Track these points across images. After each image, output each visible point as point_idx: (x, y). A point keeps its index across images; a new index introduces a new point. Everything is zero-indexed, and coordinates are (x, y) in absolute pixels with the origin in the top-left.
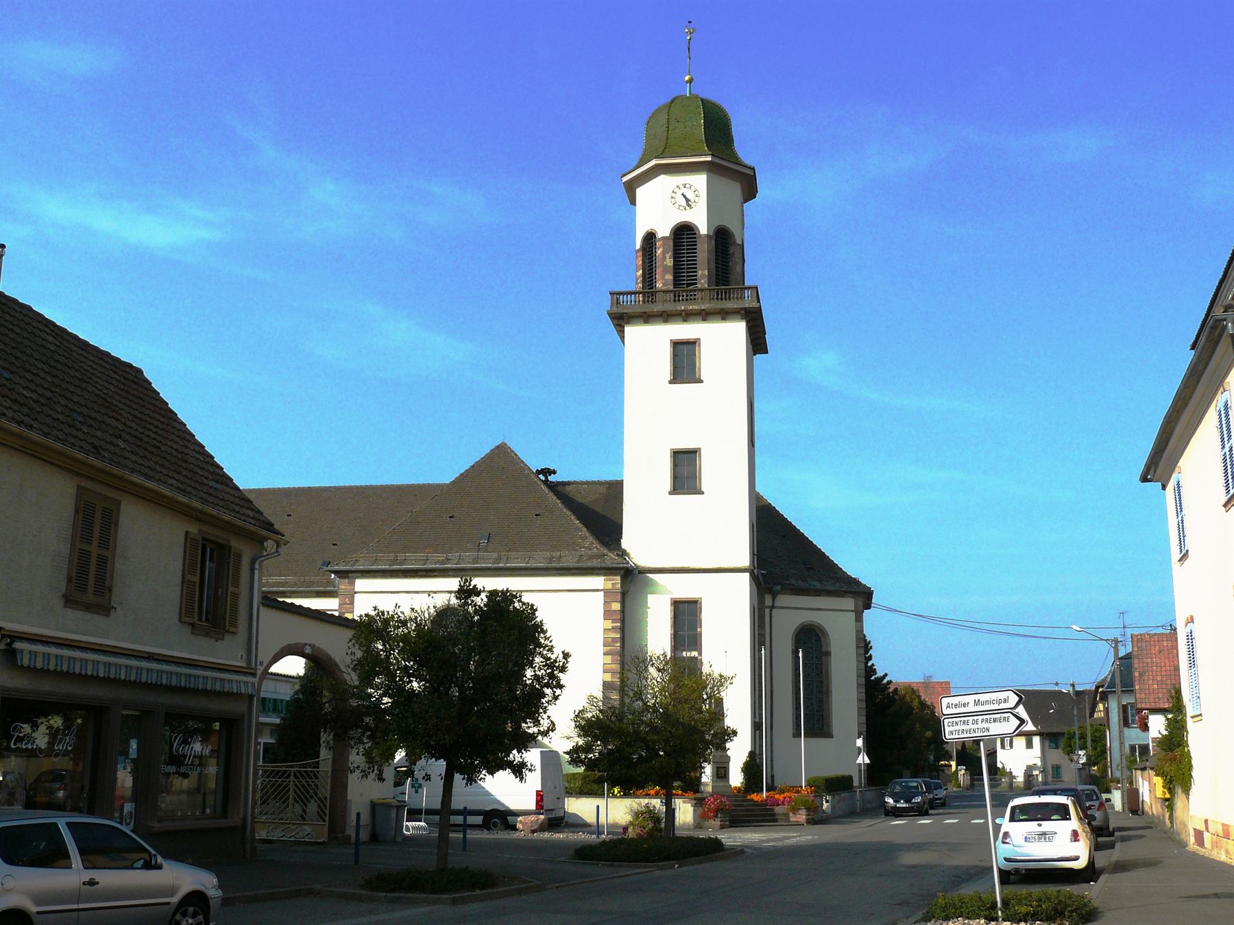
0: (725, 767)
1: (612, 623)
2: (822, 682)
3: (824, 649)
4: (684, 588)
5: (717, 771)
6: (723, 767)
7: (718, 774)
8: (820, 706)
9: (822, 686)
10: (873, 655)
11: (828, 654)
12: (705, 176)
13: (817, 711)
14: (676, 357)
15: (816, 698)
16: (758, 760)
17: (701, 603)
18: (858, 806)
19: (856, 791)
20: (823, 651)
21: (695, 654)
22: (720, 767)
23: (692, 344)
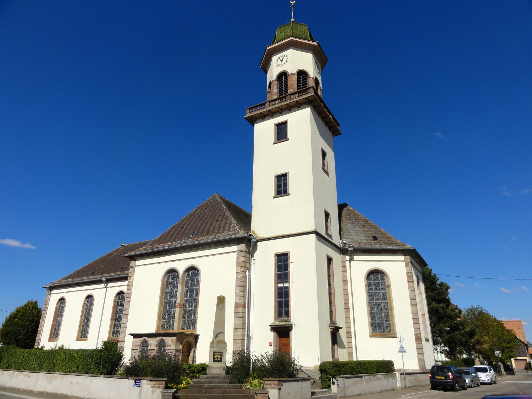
0: (222, 353)
1: (240, 269)
2: (387, 303)
3: (387, 284)
4: (281, 247)
5: (214, 355)
6: (219, 353)
7: (214, 358)
8: (387, 318)
9: (388, 306)
10: (446, 282)
11: (389, 286)
12: (309, 108)
13: (386, 321)
14: (379, 371)
15: (385, 313)
16: (511, 368)
17: (289, 254)
18: (251, 248)
19: (396, 374)
20: (386, 285)
21: (286, 285)
22: (216, 352)
23: (285, 123)
